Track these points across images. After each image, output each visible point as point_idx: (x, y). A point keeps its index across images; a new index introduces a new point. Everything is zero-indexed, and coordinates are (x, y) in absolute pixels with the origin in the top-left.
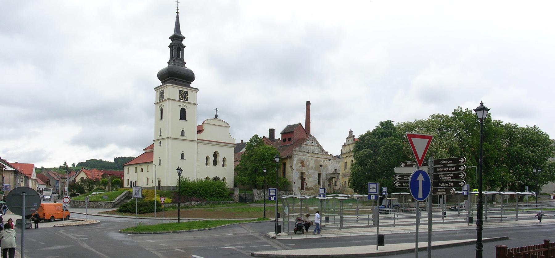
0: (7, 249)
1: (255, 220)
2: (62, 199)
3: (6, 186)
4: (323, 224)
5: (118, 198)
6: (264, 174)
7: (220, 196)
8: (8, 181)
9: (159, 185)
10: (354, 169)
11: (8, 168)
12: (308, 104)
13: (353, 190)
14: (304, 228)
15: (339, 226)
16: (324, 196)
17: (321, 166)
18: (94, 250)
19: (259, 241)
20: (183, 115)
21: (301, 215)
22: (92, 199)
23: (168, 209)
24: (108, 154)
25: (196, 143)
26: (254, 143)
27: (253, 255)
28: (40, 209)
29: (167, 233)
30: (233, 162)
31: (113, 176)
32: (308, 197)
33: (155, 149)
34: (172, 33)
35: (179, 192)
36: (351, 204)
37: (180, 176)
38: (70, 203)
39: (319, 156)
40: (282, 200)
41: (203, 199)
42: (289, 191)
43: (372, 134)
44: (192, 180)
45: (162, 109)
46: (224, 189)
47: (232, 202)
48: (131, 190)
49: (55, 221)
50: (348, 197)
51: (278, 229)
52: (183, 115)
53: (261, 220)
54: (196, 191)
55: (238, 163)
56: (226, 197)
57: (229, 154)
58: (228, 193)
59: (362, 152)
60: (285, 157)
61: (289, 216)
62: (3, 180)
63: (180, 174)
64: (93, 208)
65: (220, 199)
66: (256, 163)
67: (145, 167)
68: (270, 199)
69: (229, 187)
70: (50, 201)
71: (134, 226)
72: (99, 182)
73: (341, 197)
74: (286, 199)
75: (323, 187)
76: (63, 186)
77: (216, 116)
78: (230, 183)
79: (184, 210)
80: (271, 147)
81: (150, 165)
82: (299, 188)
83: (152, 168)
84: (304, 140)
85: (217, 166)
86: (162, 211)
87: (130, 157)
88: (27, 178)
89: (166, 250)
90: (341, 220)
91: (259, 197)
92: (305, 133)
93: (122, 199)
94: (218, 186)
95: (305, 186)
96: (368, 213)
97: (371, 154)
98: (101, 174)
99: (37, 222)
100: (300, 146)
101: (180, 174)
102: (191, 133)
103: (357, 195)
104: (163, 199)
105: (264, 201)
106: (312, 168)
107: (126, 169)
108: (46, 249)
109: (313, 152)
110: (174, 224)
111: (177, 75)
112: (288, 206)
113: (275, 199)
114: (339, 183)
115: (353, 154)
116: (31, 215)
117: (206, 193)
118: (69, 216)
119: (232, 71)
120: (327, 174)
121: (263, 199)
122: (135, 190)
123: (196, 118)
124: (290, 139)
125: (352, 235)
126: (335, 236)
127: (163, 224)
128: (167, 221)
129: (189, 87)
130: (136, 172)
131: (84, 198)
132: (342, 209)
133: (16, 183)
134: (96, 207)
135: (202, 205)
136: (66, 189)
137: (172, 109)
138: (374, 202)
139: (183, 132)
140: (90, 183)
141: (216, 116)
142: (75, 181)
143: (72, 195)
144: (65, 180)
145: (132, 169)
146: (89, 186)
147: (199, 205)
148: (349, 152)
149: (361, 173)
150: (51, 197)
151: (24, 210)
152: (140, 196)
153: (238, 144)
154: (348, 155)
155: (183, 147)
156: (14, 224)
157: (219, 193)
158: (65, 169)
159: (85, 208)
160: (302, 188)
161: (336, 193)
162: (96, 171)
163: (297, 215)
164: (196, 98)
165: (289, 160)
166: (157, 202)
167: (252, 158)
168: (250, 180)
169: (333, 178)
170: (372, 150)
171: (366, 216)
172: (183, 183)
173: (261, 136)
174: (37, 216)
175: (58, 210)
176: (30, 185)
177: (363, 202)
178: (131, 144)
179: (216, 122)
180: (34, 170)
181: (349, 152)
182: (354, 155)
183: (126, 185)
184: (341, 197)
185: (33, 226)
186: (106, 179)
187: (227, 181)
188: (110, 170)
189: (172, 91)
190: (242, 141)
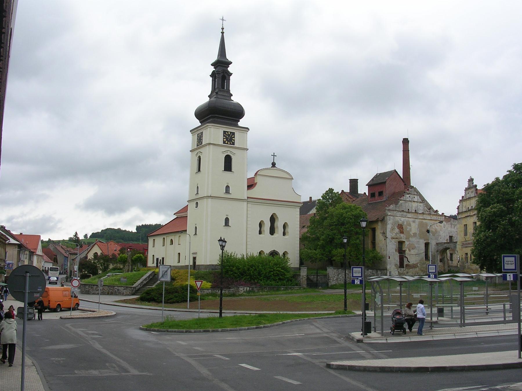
0: (7, 345)
1: (331, 314)
2: (71, 281)
3: (9, 264)
4: (434, 319)
5: (139, 282)
6: (343, 245)
7: (280, 279)
8: (11, 257)
9: (194, 263)
10: (478, 234)
11: (12, 241)
12: (406, 142)
13: (478, 267)
14: (406, 326)
15: (459, 322)
16: (435, 277)
17: (428, 231)
18: (108, 353)
19: (338, 345)
20: (228, 165)
21: (401, 306)
22: (107, 283)
23: (206, 298)
24: (128, 222)
25: (245, 203)
26: (327, 200)
27: (329, 366)
28: (45, 294)
29: (204, 331)
30: (298, 229)
31: (134, 251)
32: (411, 279)
33: (189, 213)
34: (215, 58)
35: (221, 273)
36: (477, 288)
37: (222, 249)
38: (80, 286)
39: (425, 217)
40: (371, 284)
41: (255, 284)
42: (381, 270)
43: (502, 181)
44: (239, 256)
45: (200, 157)
46: (286, 269)
47: (296, 288)
48: (157, 270)
49: (61, 311)
50: (472, 277)
51: (367, 328)
52: (228, 165)
53: (340, 313)
54: (245, 272)
55: (305, 230)
56: (288, 280)
57: (292, 218)
58: (292, 273)
59: (489, 208)
60: (374, 219)
61: (382, 308)
62: (6, 257)
63: (223, 247)
64: (108, 294)
65: (280, 283)
66: (332, 230)
67: (175, 238)
68: (353, 282)
69: (292, 266)
70: (56, 283)
71: (160, 320)
72: (116, 258)
73: (461, 277)
74: (377, 281)
75: (433, 263)
76: (72, 265)
77: (274, 165)
78: (293, 260)
79: (228, 298)
80: (353, 205)
81: (182, 235)
82: (396, 265)
83: (185, 239)
84: (402, 194)
85: (275, 235)
86: (197, 300)
87: (156, 225)
88: (32, 254)
89: (204, 356)
90: (463, 313)
91: (337, 279)
92: (402, 184)
93: (145, 282)
94: (276, 264)
95: (406, 263)
96: (502, 301)
97: (503, 211)
98: (119, 248)
99: (40, 312)
100: (396, 203)
101: (223, 247)
102: (240, 190)
103: (484, 275)
104: (199, 284)
105: (345, 286)
106: (415, 234)
107: (151, 241)
108: (50, 347)
109: (416, 212)
110: (214, 319)
111: (221, 112)
112: (381, 292)
113: (361, 281)
114: (457, 257)
115: (476, 212)
116: (35, 302)
117: (259, 274)
118: (78, 304)
119: (295, 100)
120: (437, 244)
121: (343, 283)
122: (161, 270)
123: (245, 169)
124: (381, 194)
125: (479, 336)
126: (454, 337)
127: (199, 319)
128: (205, 314)
129: (237, 126)
130: (164, 245)
131: (97, 280)
132: (462, 296)
133: (19, 259)
134: (112, 294)
135: (254, 292)
136: (76, 268)
137: (214, 157)
138: (512, 284)
139: (228, 187)
140: (105, 260)
141: (274, 165)
142: (86, 257)
143: (83, 277)
144: (75, 257)
145: (159, 240)
146: (104, 264)
147: (249, 292)
148: (469, 210)
149: (489, 240)
150: (57, 278)
151: (27, 295)
152: (168, 279)
153: (305, 203)
154: (468, 214)
155: (226, 208)
156: (15, 313)
157: (278, 275)
158: (75, 241)
159: (98, 294)
160: (401, 265)
161: (453, 271)
162: (113, 243)
163: (394, 306)
164: (245, 140)
165: (380, 224)
166: (191, 287)
167: (326, 223)
168: (323, 254)
169: (446, 249)
170: (505, 206)
171: (500, 307)
172: (228, 261)
173: (337, 190)
174: (41, 303)
175: (65, 296)
176: (35, 264)
177: (495, 285)
178: (157, 207)
179: (273, 173)
180: (40, 243)
181: (469, 210)
182: (478, 213)
183: (150, 263)
184: (461, 277)
185: (37, 317)
186: (125, 255)
187: (289, 256)
188: (131, 243)
189: (215, 133)
190: (311, 198)
